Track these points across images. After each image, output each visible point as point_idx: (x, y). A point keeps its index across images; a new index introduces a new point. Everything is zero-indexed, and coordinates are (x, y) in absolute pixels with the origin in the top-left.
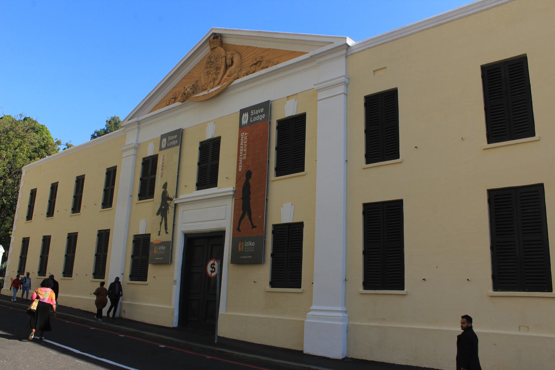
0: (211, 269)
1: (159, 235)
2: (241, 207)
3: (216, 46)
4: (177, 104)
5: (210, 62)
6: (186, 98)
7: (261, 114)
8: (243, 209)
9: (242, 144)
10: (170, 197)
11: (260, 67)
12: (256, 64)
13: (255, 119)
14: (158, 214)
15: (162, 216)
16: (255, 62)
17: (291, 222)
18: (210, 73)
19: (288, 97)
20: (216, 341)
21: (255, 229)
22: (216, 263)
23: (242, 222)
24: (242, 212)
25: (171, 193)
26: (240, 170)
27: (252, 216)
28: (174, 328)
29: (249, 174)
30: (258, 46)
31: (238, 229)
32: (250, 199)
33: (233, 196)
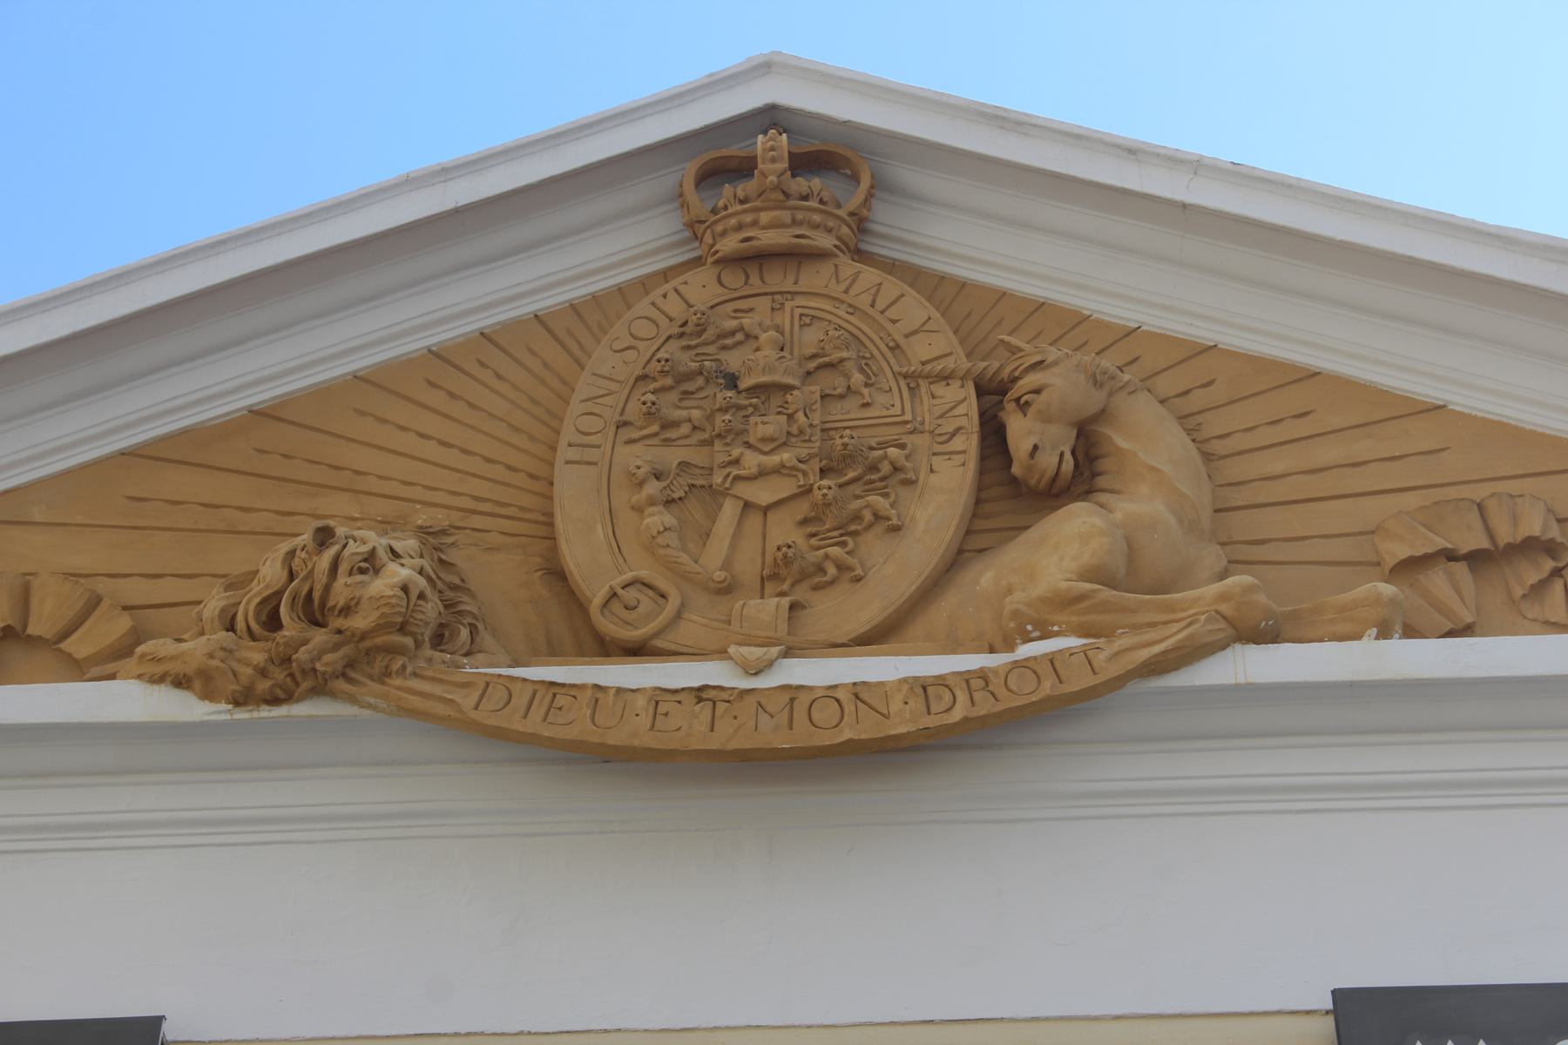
3: (824, 241)
4: (126, 700)
5: (696, 386)
12: (1475, 559)
16: (1475, 540)
18: (715, 495)
30: (1461, 400)
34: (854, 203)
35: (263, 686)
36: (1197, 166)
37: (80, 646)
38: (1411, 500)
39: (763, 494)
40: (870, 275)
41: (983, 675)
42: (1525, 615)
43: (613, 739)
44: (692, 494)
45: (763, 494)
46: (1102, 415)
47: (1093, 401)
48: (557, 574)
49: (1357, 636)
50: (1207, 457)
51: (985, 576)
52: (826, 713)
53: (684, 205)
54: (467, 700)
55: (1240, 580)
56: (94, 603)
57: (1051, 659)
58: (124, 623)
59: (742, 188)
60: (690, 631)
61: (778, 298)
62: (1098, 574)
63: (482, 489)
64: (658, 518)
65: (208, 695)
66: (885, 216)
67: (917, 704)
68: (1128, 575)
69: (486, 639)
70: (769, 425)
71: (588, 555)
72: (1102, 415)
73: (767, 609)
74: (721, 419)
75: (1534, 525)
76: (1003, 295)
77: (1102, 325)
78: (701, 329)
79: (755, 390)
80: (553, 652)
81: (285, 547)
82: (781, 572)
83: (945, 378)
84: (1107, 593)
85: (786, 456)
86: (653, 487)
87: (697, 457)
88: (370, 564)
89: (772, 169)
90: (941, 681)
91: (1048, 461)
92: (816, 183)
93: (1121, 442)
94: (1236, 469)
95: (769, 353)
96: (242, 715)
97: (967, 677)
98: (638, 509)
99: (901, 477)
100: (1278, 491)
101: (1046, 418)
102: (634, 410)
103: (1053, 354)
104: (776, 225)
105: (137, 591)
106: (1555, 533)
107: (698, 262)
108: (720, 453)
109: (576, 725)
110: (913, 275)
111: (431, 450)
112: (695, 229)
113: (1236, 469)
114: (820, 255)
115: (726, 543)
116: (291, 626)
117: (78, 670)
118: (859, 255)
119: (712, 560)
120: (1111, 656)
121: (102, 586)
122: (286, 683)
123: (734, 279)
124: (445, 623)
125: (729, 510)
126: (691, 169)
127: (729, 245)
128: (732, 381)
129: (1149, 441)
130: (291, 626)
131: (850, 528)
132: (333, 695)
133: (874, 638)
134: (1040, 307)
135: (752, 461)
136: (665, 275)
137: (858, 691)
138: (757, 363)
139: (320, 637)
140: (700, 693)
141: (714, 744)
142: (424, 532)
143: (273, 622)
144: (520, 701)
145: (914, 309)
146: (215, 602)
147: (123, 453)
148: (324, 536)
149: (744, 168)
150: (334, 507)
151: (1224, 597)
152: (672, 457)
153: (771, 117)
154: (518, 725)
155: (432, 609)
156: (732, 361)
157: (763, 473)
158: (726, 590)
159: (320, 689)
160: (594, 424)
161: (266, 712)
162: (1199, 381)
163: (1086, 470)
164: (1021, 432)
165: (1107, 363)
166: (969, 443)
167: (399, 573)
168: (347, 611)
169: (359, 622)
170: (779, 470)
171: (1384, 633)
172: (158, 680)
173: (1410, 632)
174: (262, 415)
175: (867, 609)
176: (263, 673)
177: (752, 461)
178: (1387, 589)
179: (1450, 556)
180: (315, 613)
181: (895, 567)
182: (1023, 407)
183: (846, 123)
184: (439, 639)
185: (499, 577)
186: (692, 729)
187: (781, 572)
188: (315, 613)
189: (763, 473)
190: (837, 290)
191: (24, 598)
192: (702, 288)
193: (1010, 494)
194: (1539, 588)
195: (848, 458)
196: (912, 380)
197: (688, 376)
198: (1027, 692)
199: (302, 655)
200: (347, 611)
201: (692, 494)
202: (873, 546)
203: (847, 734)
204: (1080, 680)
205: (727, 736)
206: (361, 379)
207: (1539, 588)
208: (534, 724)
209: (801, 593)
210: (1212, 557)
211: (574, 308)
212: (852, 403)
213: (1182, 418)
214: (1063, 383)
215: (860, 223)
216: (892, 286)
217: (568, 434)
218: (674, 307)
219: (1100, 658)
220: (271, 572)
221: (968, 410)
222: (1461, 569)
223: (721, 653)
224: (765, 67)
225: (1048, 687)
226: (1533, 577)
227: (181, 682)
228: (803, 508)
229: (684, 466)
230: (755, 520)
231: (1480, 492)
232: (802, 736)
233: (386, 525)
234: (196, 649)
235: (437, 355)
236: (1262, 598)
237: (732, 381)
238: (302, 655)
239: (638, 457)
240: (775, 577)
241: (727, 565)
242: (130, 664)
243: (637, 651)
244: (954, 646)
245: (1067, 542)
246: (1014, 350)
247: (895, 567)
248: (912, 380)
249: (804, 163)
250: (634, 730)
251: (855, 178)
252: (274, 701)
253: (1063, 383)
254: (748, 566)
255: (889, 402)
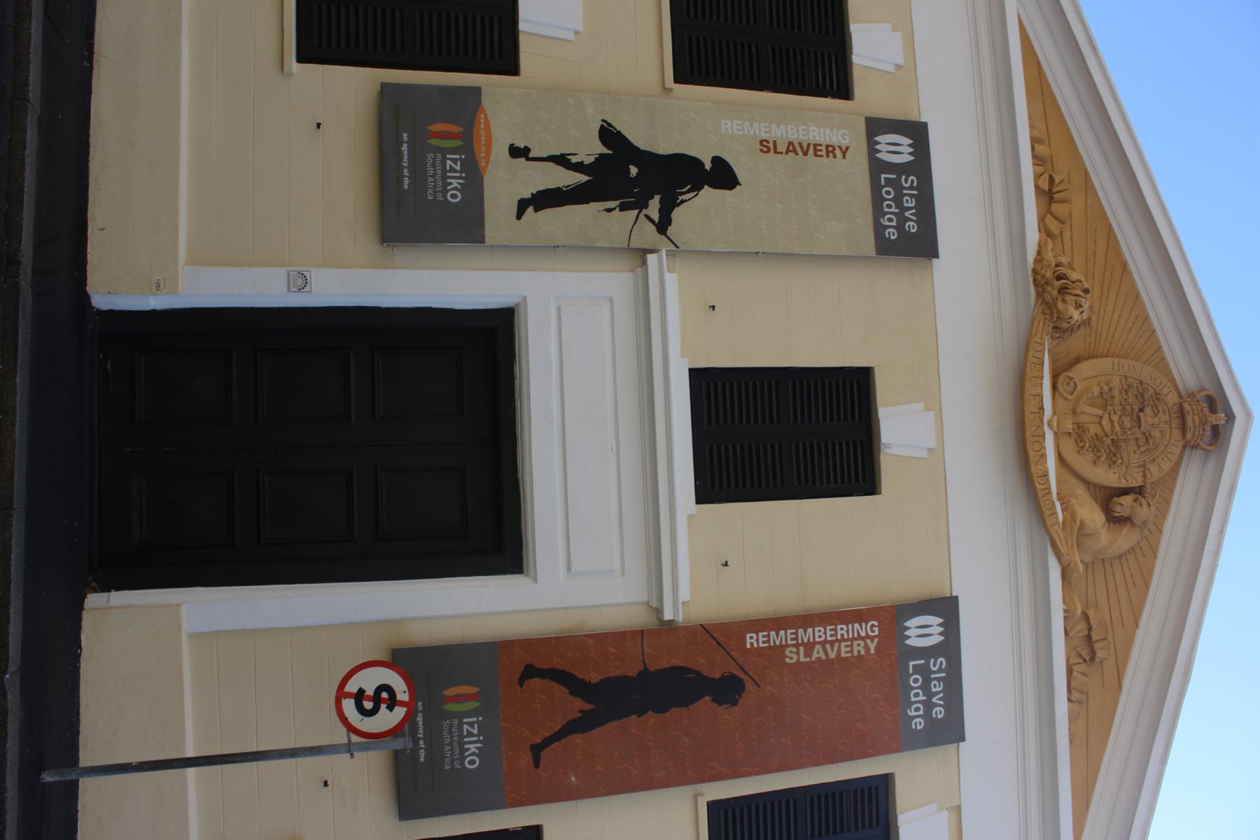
0: (370, 692)
1: (517, 152)
2: (614, 672)
3: (1189, 436)
4: (1033, 236)
5: (1138, 400)
6: (1050, 288)
7: (902, 220)
8: (609, 684)
9: (842, 630)
10: (677, 214)
11: (1074, 660)
12: (1089, 637)
13: (915, 681)
14: (608, 134)
15: (595, 168)
16: (1095, 636)
17: (522, 26)
18: (1104, 407)
19: (959, 808)
20: (48, 777)
21: (526, 759)
22: (400, 712)
23: (556, 686)
24: (594, 677)
25: (700, 210)
26: (751, 640)
27: (577, 739)
28: (87, 298)
29: (728, 690)
30: (1140, 634)
31: (530, 672)
32: (641, 713)
33: (662, 622)
34: (1202, 444)
35: (1039, 277)
36: (1217, 553)
37: (1049, 219)
38: (1107, 618)
39: (1105, 422)
40: (1177, 451)
41: (1050, 492)
42: (1070, 650)
43: (1027, 384)
44: (1104, 401)
45: (1105, 422)
46: (1133, 524)
47: (1138, 520)
48: (1078, 360)
49: (1064, 602)
50: (1120, 556)
51: (1081, 491)
52: (1037, 446)
53: (1200, 392)
54: (1037, 339)
55: (1081, 568)
56: (1062, 222)
57: (1055, 513)
58: (1056, 232)
59: (1206, 410)
60: (1060, 402)
61: (1169, 423)
62: (1082, 523)
63: (1104, 334)
64: (1096, 391)
65: (1036, 261)
66: (1197, 454)
67: (1041, 473)
68: (1082, 534)
69: (1056, 341)
70: (1127, 422)
71: (1084, 370)
72: (1133, 524)
73: (1069, 425)
74: (1128, 408)
75: (1100, 654)
76: (1172, 491)
77: (1162, 523)
78: (1158, 400)
79: (1139, 418)
80: (1053, 361)
81: (1082, 279)
82: (1080, 429)
83: (1144, 476)
84: (1076, 529)
85: (1117, 428)
86: (1106, 388)
87: (1117, 401)
88: (1078, 306)
89: (1213, 419)
90: (1048, 480)
91: (1118, 508)
92: (1209, 433)
93: (1125, 530)
94: (1117, 566)
95: (1151, 421)
96: (1030, 272)
97: (1049, 488)
98: (1099, 384)
99: (1112, 463)
100: (1110, 577)
101: (1132, 507)
102: (1131, 381)
103: (1153, 509)
104: (1194, 421)
105: (1067, 235)
106: (1098, 660)
107: (1181, 396)
108: (1118, 408)
109: (1031, 372)
110: (1178, 463)
111: (1116, 318)
112: (1192, 395)
113: (1117, 566)
114: (1184, 434)
115: (1089, 412)
116: (1058, 284)
117: (1041, 220)
118: (1185, 446)
119: (1084, 408)
120: (1058, 532)
121: (1068, 224)
122: (1040, 283)
123: (1175, 409)
124: (1060, 328)
125: (1100, 412)
126: (1212, 393)
127: (1187, 407)
128: (1141, 410)
129: (1125, 539)
130: (1058, 284)
131: (1095, 449)
132: (1037, 299)
133: (1061, 458)
134: (1168, 503)
135: (1115, 418)
136: (1176, 386)
137: (1044, 456)
138: (1147, 418)
139: (1055, 293)
140: (1042, 408)
141: (1027, 414)
142: (1089, 319)
143: (1059, 278)
144: (1038, 355)
145: (1167, 465)
146: (1064, 260)
147: (1110, 225)
148: (1086, 291)
149: (1213, 410)
150: (1096, 292)
151: (1076, 564)
152: (1116, 393)
153: (1231, 417)
154: (1030, 354)
155: (1065, 325)
156: (1148, 410)
157: (1112, 422)
158: (1074, 412)
159: (1039, 294)
160: (1126, 369)
161: (1031, 279)
162: (1147, 551)
163: (1114, 520)
164: (1127, 500)
165: (1150, 526)
166: (1123, 484)
167: (1076, 314)
168: (1063, 300)
169: (1060, 305)
170: (1113, 426)
171: (1065, 611)
172: (1039, 245)
173: (1066, 618)
174: (1125, 266)
175: (1069, 455)
176: (1043, 277)
177: (1115, 418)
178: (1079, 612)
179: (1090, 629)
180: (1062, 290)
181: (1082, 463)
182: (1135, 501)
183: (1229, 441)
184: (1055, 327)
185: (1075, 344)
186: (1031, 407)
187: (1080, 429)
188: (1062, 290)
189: (1112, 422)
190: (1172, 441)
191: (1063, 201)
192: (1172, 399)
193: (1107, 498)
194: (1080, 655)
195: (1117, 448)
196: (1143, 466)
197: (1142, 397)
198: (1045, 506)
199: (1049, 288)
200: (1063, 300)
201: (1104, 401)
202: (1090, 456)
203: (1031, 453)
204: (1049, 521)
205: (1029, 418)
206: (1138, 295)
207: (1080, 655)
208: (1031, 359)
209: (1074, 436)
210: (1088, 559)
211: (1164, 359)
212: (1135, 448)
213: (1133, 548)
214: (1143, 512)
215: (1195, 447)
216: (1174, 458)
217: (1122, 361)
218: (1165, 391)
219: (1056, 527)
220: (1075, 276)
221: (1134, 484)
222: (1086, 632)
223: (1054, 413)
224: (1248, 415)
225: (1047, 512)
226: (1084, 654)
227: (1039, 253)
228: (1101, 434)
229: (1113, 397)
230: (1097, 420)
231: (1110, 639)
232: (1030, 440)
233: (1091, 307)
234: (1049, 256)
235: (1147, 317)
236: (1075, 575)
237: (1141, 410)
238: (1049, 288)
239: (1116, 383)
240: (1079, 427)
241: (1082, 412)
242: (1044, 236)
243: (1054, 387)
244: (1059, 482)
245: (1092, 515)
246: (1154, 497)
247: (1082, 463)
248: (1143, 466)
249: (1216, 431)
250: (1030, 390)
251: (1210, 445)
252: (1035, 281)
253: (1143, 512)
254: (1081, 419)
255: (1136, 459)
